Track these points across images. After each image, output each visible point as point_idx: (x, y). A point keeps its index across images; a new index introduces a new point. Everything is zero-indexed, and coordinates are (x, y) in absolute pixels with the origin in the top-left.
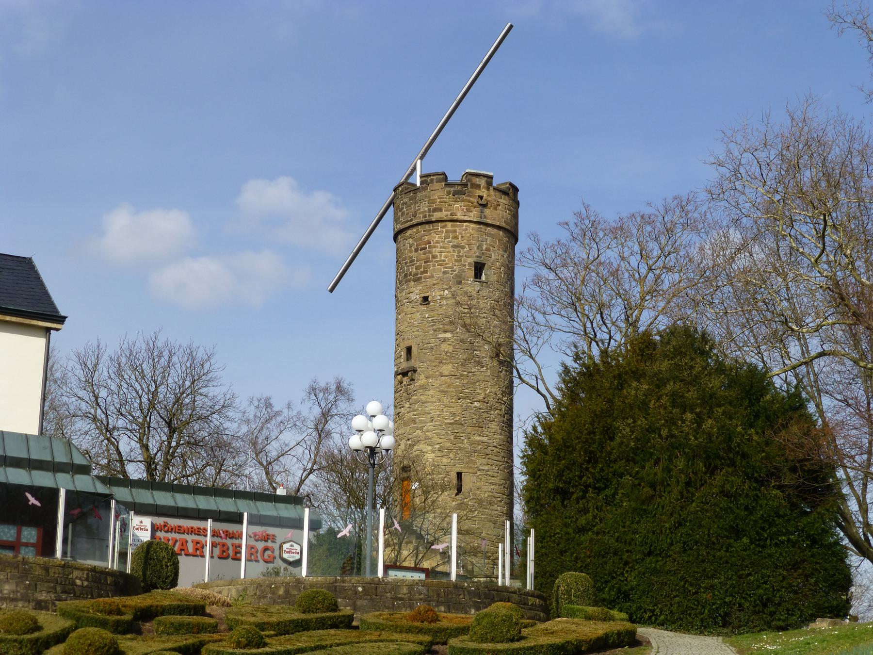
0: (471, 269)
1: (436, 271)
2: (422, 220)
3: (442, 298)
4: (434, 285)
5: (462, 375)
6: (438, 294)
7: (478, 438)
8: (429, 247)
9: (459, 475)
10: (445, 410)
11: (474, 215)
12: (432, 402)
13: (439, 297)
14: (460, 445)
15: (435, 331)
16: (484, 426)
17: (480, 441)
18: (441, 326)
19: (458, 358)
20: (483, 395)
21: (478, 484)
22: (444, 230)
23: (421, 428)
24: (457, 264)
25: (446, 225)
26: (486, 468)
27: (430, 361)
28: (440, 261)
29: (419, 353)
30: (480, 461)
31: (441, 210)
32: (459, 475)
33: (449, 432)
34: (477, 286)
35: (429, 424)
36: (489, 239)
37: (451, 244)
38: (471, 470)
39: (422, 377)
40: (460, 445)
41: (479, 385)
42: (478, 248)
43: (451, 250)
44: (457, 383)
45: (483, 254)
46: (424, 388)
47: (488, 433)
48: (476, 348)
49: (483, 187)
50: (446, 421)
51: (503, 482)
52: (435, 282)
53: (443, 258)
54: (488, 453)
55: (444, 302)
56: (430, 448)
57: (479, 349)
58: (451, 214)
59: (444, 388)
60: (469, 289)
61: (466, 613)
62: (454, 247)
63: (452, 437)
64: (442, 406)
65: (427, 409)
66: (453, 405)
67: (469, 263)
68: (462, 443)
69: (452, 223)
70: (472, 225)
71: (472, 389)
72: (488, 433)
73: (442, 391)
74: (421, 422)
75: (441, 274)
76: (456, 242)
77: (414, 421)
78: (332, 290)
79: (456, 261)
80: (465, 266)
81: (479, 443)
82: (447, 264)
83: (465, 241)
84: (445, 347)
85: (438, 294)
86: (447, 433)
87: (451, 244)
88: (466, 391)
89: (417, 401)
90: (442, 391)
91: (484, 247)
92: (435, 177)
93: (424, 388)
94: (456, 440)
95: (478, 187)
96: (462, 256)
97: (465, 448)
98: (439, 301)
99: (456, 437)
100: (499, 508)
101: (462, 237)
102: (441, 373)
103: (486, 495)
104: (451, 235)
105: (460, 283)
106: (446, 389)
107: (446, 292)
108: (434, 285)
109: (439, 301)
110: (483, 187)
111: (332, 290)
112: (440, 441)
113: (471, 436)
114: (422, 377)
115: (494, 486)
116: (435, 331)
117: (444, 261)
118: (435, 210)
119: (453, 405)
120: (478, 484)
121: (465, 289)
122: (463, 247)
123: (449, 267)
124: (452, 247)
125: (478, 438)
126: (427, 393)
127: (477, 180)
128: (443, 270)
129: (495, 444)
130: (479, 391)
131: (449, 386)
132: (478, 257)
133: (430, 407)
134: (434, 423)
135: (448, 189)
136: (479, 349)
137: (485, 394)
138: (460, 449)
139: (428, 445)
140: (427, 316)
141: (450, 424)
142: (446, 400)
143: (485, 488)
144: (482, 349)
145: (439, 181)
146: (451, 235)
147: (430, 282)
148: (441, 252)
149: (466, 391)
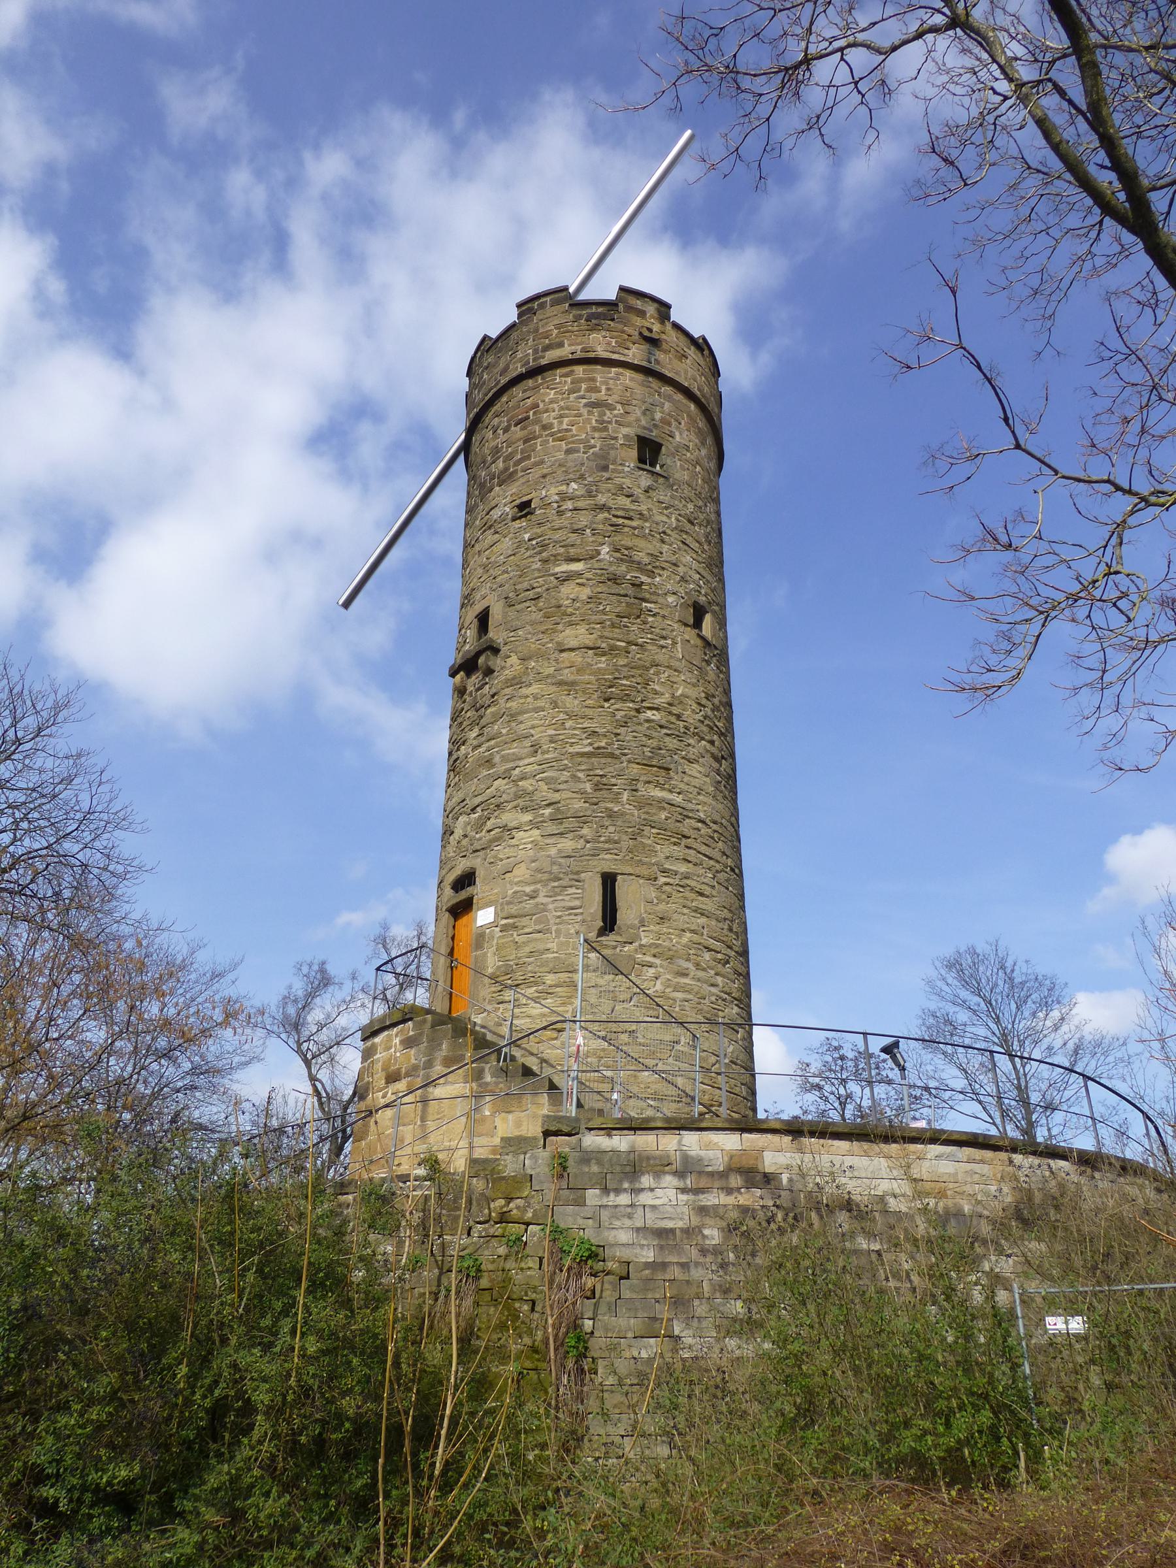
0: (629, 446)
1: (551, 452)
2: (521, 370)
3: (564, 497)
4: (544, 477)
5: (613, 648)
6: (553, 490)
7: (658, 793)
8: (534, 413)
9: (609, 881)
10: (569, 724)
11: (635, 353)
12: (537, 710)
13: (556, 498)
14: (610, 805)
15: (545, 561)
16: (672, 766)
17: (663, 800)
18: (562, 550)
19: (603, 612)
20: (667, 697)
21: (662, 907)
22: (569, 380)
23: (506, 775)
24: (596, 435)
25: (573, 371)
26: (683, 868)
27: (532, 623)
28: (559, 431)
29: (505, 615)
30: (664, 850)
31: (561, 345)
32: (609, 881)
33: (580, 775)
34: (645, 480)
35: (526, 761)
36: (667, 405)
37: (584, 401)
38: (644, 871)
39: (514, 659)
40: (610, 805)
41: (657, 674)
42: (644, 413)
43: (584, 411)
44: (602, 663)
45: (655, 426)
46: (516, 682)
47: (682, 786)
48: (647, 596)
49: (652, 317)
50: (571, 750)
51: (726, 914)
52: (545, 471)
53: (565, 427)
54: (686, 832)
55: (569, 505)
56: (528, 817)
57: (654, 598)
58: (584, 350)
59: (567, 675)
60: (627, 482)
61: (476, 1352)
62: (593, 405)
63: (588, 787)
64: (562, 716)
65: (522, 726)
66: (589, 712)
67: (625, 436)
68: (616, 799)
69: (585, 367)
70: (628, 373)
71: (639, 680)
72: (682, 786)
73: (560, 683)
74: (505, 759)
75: (561, 456)
76: (594, 397)
77: (489, 762)
78: (347, 604)
79: (594, 429)
80: (616, 438)
81: (662, 804)
82: (573, 436)
83: (616, 397)
84: (568, 590)
85: (553, 490)
86: (574, 776)
87: (584, 401)
88: (624, 682)
89: (497, 717)
90: (560, 683)
91: (658, 416)
92: (548, 299)
93: (516, 682)
94: (598, 794)
95: (642, 314)
96: (610, 422)
97: (623, 814)
98: (555, 505)
99: (597, 787)
100: (719, 980)
101: (608, 389)
102: (558, 643)
103: (685, 940)
104: (584, 386)
105: (605, 468)
106: (571, 678)
107: (574, 485)
108: (544, 477)
109: (555, 505)
110: (652, 317)
111: (347, 604)
112: (557, 797)
113: (640, 786)
114: (514, 659)
115: (703, 921)
116: (545, 561)
117: (567, 430)
118: (547, 348)
119: (589, 712)
120: (662, 907)
121: (618, 481)
122: (611, 408)
123: (580, 441)
124: (586, 405)
125: (658, 793)
126: (524, 691)
127: (638, 303)
128: (564, 447)
129: (702, 815)
130: (657, 687)
131: (580, 671)
132: (645, 428)
133: (529, 720)
134: (539, 757)
135: (575, 312)
136: (654, 598)
137: (673, 696)
138: (611, 815)
139: (525, 809)
140: (527, 536)
141: (583, 755)
142: (572, 703)
143: (681, 920)
144: (660, 600)
145: (555, 303)
146: (584, 386)
147: (536, 473)
148: (561, 416)
149: (624, 682)
